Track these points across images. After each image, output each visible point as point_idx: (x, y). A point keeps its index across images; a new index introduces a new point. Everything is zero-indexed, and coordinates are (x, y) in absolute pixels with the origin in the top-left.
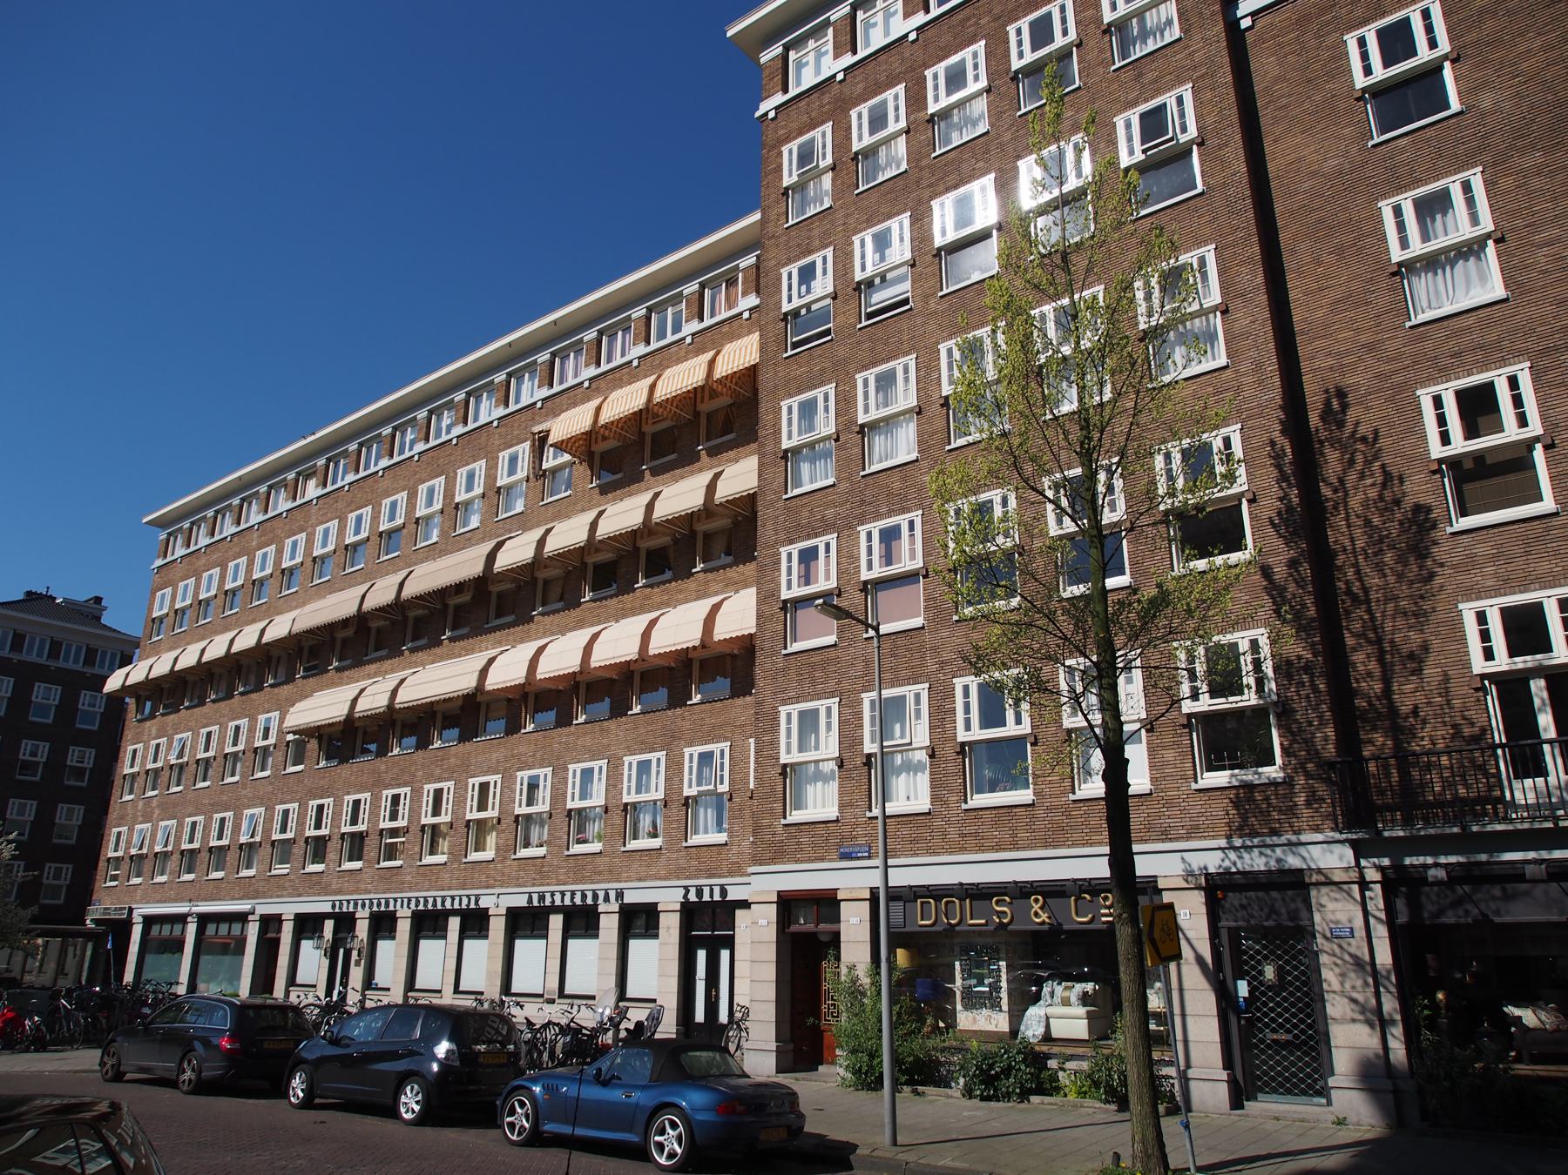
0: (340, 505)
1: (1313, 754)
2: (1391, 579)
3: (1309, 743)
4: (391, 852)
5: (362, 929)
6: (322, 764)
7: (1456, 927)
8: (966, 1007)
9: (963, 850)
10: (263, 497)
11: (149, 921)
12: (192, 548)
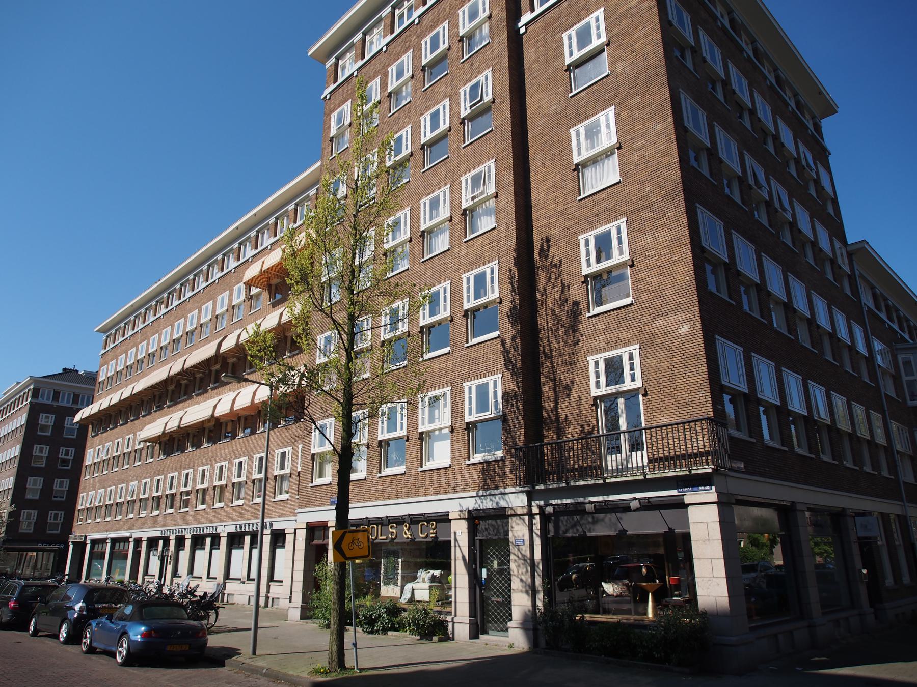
0: (172, 318)
1: (515, 444)
2: (562, 344)
3: (513, 437)
4: (186, 504)
5: (172, 544)
6: (161, 457)
7: (573, 538)
8: (385, 584)
9: (377, 499)
10: (254, 239)
11: (94, 542)
12: (225, 271)
